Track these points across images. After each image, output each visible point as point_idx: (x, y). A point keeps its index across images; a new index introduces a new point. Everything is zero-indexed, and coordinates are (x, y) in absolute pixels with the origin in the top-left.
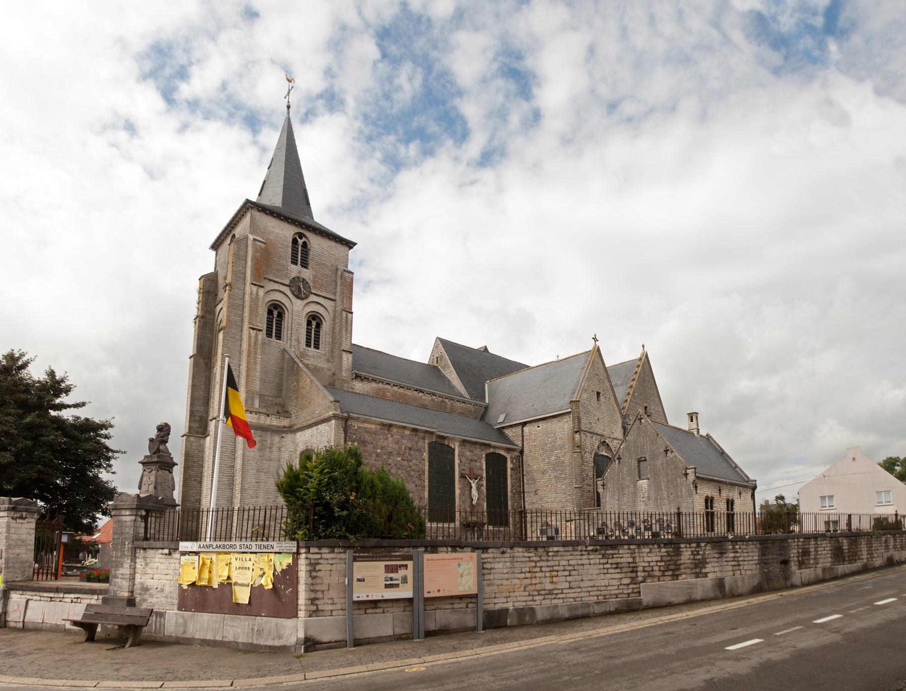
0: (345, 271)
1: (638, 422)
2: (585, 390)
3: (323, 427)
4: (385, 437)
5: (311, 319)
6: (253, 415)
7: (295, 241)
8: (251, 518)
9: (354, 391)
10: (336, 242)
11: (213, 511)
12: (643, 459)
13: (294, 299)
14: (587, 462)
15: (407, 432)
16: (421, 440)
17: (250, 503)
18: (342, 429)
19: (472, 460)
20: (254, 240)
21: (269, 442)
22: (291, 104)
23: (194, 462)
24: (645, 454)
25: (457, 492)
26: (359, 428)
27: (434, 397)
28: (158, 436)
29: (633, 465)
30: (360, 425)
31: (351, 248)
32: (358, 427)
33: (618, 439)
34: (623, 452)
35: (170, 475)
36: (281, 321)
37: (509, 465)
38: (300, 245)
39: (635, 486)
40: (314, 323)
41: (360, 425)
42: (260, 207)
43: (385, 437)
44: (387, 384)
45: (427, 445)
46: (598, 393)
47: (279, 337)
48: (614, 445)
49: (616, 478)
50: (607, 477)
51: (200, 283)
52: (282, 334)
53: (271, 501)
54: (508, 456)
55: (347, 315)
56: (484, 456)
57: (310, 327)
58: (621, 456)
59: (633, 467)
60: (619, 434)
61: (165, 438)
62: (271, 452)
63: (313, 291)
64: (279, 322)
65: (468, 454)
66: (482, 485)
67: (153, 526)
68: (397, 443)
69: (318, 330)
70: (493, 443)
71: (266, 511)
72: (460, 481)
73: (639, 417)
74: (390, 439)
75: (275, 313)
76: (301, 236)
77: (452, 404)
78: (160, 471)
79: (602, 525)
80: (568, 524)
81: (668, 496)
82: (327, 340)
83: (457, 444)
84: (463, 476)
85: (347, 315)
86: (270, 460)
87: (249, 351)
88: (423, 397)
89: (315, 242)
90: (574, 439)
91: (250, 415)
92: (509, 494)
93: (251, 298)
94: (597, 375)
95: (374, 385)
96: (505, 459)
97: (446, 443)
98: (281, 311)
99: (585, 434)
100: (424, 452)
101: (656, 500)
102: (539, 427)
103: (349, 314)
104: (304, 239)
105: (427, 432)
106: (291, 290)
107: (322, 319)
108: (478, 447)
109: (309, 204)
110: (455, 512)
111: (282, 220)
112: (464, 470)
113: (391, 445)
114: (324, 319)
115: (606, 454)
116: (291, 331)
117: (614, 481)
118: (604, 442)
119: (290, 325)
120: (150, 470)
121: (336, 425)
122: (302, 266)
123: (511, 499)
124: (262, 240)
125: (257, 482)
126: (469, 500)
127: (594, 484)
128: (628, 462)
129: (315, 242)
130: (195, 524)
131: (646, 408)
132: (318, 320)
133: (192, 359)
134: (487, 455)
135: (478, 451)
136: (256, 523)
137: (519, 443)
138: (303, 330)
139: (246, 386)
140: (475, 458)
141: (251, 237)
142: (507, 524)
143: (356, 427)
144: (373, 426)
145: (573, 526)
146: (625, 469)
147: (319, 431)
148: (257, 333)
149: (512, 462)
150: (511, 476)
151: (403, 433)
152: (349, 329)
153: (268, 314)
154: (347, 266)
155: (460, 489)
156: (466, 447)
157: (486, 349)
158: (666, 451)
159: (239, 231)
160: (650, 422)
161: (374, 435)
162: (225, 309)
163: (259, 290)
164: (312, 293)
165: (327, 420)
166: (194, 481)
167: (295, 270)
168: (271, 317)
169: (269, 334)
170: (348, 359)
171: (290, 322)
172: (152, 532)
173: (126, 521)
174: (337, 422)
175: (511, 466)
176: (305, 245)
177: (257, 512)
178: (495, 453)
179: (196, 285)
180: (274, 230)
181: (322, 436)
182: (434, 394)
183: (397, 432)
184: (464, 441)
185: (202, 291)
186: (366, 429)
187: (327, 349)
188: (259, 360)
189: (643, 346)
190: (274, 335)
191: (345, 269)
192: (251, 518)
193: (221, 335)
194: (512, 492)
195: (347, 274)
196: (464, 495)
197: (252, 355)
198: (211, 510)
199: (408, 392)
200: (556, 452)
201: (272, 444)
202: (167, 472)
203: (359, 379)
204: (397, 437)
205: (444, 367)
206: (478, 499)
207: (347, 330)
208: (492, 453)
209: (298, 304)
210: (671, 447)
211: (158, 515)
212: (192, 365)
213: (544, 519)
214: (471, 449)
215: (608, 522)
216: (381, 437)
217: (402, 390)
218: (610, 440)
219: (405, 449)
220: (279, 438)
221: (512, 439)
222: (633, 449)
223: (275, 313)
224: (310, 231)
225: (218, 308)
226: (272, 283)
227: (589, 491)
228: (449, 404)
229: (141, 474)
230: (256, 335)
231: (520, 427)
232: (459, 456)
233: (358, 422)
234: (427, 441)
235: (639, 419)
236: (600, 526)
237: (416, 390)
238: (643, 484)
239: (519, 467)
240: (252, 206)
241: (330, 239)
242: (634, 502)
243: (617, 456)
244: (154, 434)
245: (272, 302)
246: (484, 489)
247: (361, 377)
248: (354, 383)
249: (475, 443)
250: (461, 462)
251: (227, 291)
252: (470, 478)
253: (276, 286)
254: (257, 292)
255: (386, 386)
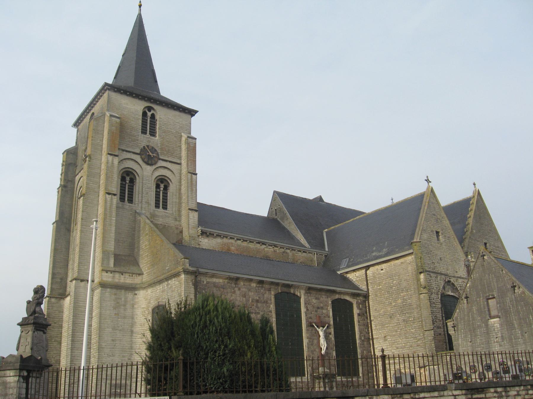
0: (188, 137)
1: (480, 259)
2: (424, 230)
3: (173, 282)
4: (233, 290)
5: (159, 183)
6: (109, 274)
7: (144, 114)
8: (109, 377)
9: (201, 247)
10: (180, 111)
11: (83, 370)
12: (491, 297)
13: (144, 166)
14: (434, 303)
15: (254, 285)
16: (267, 292)
17: (107, 361)
18: (191, 284)
19: (318, 308)
20: (111, 116)
21: (123, 299)
22: (142, 3)
23: (55, 323)
24: (493, 291)
25: (305, 341)
26: (208, 283)
27: (276, 248)
28: (34, 298)
29: (482, 303)
30: (208, 280)
31: (193, 115)
32: (207, 282)
33: (463, 278)
34: (470, 290)
35: (44, 336)
36: (133, 186)
37: (356, 311)
38: (149, 117)
39: (487, 325)
40: (162, 186)
41: (209, 280)
42: (116, 88)
43: (233, 290)
44: (231, 238)
45: (273, 297)
46: (437, 233)
47: (131, 200)
48: (458, 283)
49: (466, 318)
50: (457, 318)
51: (63, 156)
52: (134, 198)
53: (126, 359)
54: (354, 302)
55: (192, 176)
56: (330, 302)
57: (158, 190)
58: (468, 295)
59: (482, 306)
60: (462, 272)
61: (40, 300)
62: (125, 310)
63: (161, 157)
64: (131, 187)
65: (314, 301)
66: (330, 334)
67: (33, 387)
68: (244, 296)
69: (166, 192)
70: (338, 289)
71: (137, 367)
72: (307, 330)
73: (481, 254)
74: (238, 292)
75: (128, 179)
76: (150, 109)
77: (293, 254)
78: (36, 332)
79: (457, 370)
80: (422, 370)
81: (522, 335)
82: (175, 200)
83: (303, 292)
84: (310, 325)
85: (192, 176)
86: (125, 317)
87: (105, 214)
88: (266, 249)
89: (161, 113)
90: (418, 280)
91: (106, 274)
92: (358, 341)
93: (107, 167)
94: (434, 215)
95: (219, 240)
96: (351, 304)
97: (292, 291)
98: (132, 177)
99: (430, 275)
100: (271, 304)
101: (511, 339)
102: (382, 270)
103: (193, 176)
104: (152, 112)
105: (272, 283)
106: (141, 157)
107: (169, 182)
108: (323, 293)
109: (156, 82)
110: (358, 359)
111: (134, 97)
112: (311, 318)
113: (238, 298)
114: (171, 182)
115: (452, 294)
116: (142, 194)
117: (464, 322)
118: (449, 281)
119: (141, 189)
120: (27, 331)
121: (186, 281)
122: (151, 135)
123: (361, 347)
124: (117, 116)
125: (113, 340)
126: (317, 350)
127: (444, 326)
128: (476, 301)
129: (161, 113)
130: (54, 386)
131: (485, 244)
132: (166, 183)
133: (55, 225)
134: (333, 302)
135: (323, 298)
136: (114, 382)
137: (364, 287)
138: (152, 193)
139: (102, 246)
140: (322, 305)
141: (108, 114)
142: (356, 374)
143: (205, 282)
144: (221, 281)
145: (427, 373)
146: (474, 308)
147: (169, 286)
148: (112, 198)
149: (358, 307)
150: (359, 322)
151: (250, 285)
152: (194, 189)
153: (121, 180)
154: (190, 134)
155: (308, 338)
156: (312, 295)
157: (320, 199)
158: (514, 287)
159: (96, 109)
160: (494, 259)
161: (222, 290)
162: (85, 178)
163: (114, 159)
164: (160, 159)
165: (176, 275)
166: (54, 342)
167: (144, 140)
168: (124, 183)
169: (122, 199)
170: (194, 217)
171: (141, 187)
172: (33, 392)
173: (10, 383)
174: (187, 276)
175: (358, 311)
176: (153, 116)
177: (114, 369)
178: (341, 299)
179: (59, 160)
180: (128, 106)
181: (172, 291)
182: (275, 246)
183: (244, 285)
184: (310, 289)
185: (64, 164)
186: (214, 283)
187: (174, 209)
188: (114, 221)
189: (474, 184)
190: (126, 199)
191: (189, 135)
192: (109, 377)
193: (81, 202)
194: (360, 339)
195: (190, 140)
196: (312, 345)
197: (108, 218)
198: (82, 368)
199: (251, 245)
200: (402, 294)
201: (126, 301)
202: (42, 333)
203: (205, 235)
204: (244, 289)
205: (282, 219)
206: (327, 348)
207: (192, 190)
208: (338, 299)
209: (148, 169)
210: (517, 283)
211: (38, 376)
212: (55, 230)
213: (397, 367)
214: (317, 296)
215: (463, 367)
216: (229, 290)
217: (245, 244)
218: (454, 279)
219: (252, 301)
220: (132, 296)
221: (357, 283)
222: (480, 287)
223: (128, 179)
224: (157, 104)
225: (77, 178)
226: (125, 152)
227: (440, 334)
228: (290, 254)
229: (19, 336)
230: (112, 199)
231: (364, 271)
232: (305, 304)
233: (206, 276)
234: (273, 293)
235: (481, 256)
236: (455, 371)
237: (259, 243)
238: (495, 322)
239: (366, 313)
240: (109, 88)
241: (175, 110)
242: (488, 343)
243: (464, 296)
244: (30, 296)
245: (124, 170)
246: (332, 337)
247: (206, 233)
248: (200, 240)
249: (321, 290)
250: (307, 310)
251: (87, 162)
252: (318, 327)
253: (129, 155)
254: (113, 161)
255: (232, 241)
